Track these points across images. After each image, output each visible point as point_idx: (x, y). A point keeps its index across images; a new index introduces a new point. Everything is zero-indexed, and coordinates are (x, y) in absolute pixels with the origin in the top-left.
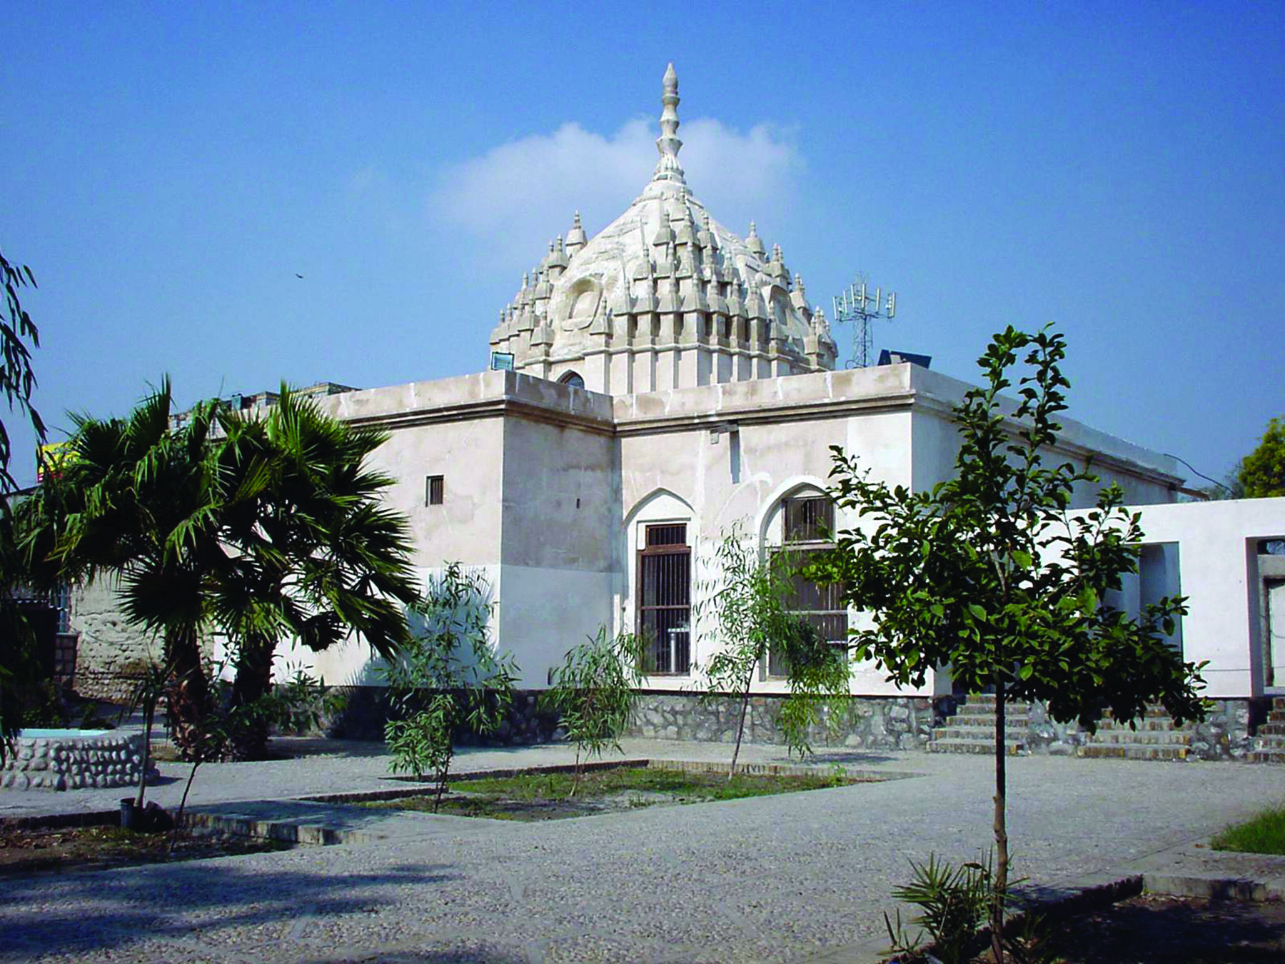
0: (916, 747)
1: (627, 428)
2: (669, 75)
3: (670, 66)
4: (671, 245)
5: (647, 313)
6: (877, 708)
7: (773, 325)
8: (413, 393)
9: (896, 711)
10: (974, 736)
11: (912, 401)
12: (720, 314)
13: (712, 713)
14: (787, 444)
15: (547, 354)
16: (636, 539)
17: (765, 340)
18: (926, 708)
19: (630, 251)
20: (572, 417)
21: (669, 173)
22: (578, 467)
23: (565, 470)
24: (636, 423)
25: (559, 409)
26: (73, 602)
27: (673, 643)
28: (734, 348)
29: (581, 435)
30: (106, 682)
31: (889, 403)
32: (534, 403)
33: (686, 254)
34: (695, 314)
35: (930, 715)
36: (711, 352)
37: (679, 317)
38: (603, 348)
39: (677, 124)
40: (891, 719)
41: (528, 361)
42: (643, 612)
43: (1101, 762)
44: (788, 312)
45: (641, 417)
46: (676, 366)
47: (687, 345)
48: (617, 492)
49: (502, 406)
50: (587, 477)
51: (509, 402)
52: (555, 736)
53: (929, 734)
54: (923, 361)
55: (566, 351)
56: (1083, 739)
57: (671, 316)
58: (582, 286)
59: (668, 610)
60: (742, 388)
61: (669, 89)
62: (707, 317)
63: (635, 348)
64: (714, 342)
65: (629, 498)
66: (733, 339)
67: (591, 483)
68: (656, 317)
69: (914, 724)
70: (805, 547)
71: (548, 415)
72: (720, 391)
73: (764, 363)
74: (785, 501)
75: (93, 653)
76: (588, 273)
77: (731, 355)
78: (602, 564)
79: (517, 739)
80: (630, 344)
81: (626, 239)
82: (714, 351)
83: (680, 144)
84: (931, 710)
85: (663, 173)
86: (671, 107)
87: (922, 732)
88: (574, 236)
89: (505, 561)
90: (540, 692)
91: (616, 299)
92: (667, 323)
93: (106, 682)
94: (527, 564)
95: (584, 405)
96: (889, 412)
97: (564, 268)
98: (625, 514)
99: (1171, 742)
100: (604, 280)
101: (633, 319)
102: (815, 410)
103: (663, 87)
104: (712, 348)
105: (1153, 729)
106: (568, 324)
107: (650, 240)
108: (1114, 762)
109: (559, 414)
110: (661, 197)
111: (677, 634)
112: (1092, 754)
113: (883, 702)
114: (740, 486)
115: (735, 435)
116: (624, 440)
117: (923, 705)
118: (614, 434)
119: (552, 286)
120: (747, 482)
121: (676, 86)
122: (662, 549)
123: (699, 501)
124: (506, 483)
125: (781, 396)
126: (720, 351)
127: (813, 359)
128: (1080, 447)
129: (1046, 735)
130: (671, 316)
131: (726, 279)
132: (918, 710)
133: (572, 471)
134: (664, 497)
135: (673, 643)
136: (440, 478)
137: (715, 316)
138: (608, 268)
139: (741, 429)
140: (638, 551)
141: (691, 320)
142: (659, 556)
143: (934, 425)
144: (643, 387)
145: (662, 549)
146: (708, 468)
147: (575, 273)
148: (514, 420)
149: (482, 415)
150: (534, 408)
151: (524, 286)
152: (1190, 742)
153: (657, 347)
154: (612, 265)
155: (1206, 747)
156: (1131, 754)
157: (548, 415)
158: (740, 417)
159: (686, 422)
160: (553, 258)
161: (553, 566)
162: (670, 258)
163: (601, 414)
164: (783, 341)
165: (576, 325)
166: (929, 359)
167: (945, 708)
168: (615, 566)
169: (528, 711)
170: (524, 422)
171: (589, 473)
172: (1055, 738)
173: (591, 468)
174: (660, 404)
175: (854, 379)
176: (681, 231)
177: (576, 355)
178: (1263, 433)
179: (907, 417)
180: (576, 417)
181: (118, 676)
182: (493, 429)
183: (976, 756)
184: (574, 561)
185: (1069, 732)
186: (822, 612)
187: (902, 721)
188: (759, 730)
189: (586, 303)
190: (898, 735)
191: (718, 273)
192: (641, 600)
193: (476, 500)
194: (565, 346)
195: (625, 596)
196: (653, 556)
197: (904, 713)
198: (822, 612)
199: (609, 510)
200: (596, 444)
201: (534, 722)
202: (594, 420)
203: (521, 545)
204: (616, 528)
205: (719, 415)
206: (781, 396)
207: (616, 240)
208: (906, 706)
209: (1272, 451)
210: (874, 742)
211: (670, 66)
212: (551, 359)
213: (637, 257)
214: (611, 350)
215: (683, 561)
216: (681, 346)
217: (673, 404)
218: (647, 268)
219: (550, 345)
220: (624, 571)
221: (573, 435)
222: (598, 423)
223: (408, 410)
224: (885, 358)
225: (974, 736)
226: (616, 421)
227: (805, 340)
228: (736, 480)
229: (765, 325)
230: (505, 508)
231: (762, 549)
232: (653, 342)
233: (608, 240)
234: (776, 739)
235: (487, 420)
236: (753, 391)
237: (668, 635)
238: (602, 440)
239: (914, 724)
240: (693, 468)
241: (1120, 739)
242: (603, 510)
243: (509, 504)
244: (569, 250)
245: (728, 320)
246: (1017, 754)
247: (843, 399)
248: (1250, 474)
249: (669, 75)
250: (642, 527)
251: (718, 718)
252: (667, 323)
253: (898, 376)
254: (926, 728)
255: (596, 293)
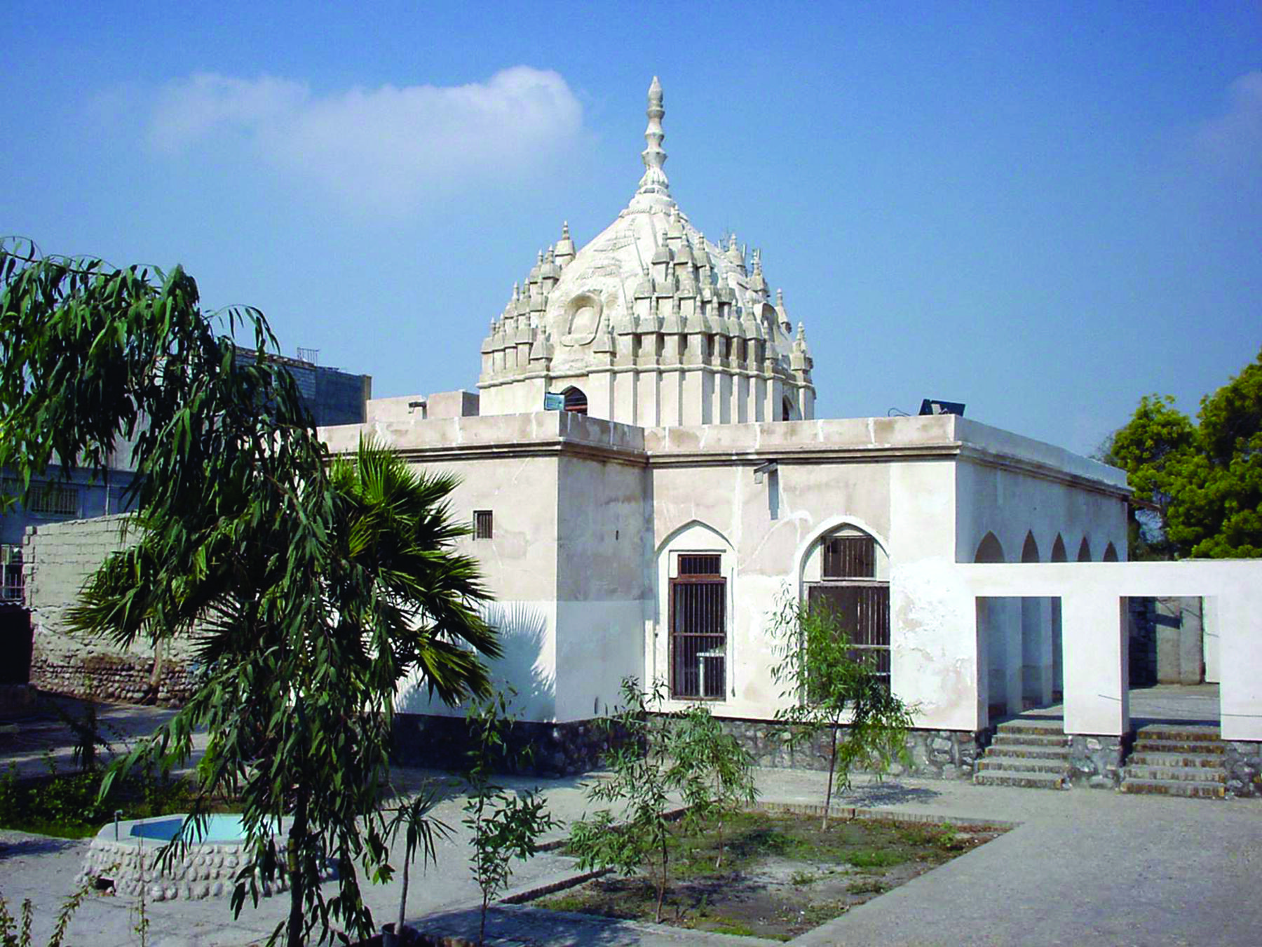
0: (959, 778)
1: (661, 460)
2: (654, 89)
3: (655, 79)
4: (671, 265)
5: (652, 333)
6: (920, 740)
7: (768, 345)
8: (457, 427)
9: (938, 743)
10: (1017, 769)
11: (958, 451)
12: (722, 335)
13: (750, 738)
14: (827, 485)
15: (548, 370)
16: (667, 568)
17: (761, 359)
18: (969, 741)
19: (626, 268)
20: (613, 452)
21: (656, 187)
22: (616, 500)
23: (608, 503)
24: (670, 456)
25: (605, 446)
26: (27, 594)
27: (702, 666)
28: (735, 369)
29: (619, 467)
30: (67, 675)
31: (934, 452)
32: (584, 442)
33: (685, 274)
34: (699, 337)
35: (972, 748)
36: (713, 373)
37: (684, 338)
38: (609, 367)
39: (662, 137)
40: (934, 750)
41: (527, 375)
42: (675, 638)
43: (1144, 799)
44: (775, 327)
45: (676, 451)
46: (680, 385)
47: (692, 366)
48: (648, 521)
49: (558, 447)
50: (623, 509)
51: (565, 444)
52: (600, 763)
53: (972, 766)
54: (957, 409)
55: (567, 366)
56: (1122, 774)
57: (676, 337)
58: (581, 302)
59: (701, 637)
60: (782, 426)
61: (655, 102)
62: (709, 338)
63: (639, 368)
64: (716, 363)
65: (661, 528)
66: (733, 358)
67: (627, 512)
68: (661, 337)
69: (957, 756)
70: (844, 584)
71: (595, 454)
72: (758, 430)
73: (760, 381)
74: (823, 539)
75: (51, 647)
76: (586, 289)
77: (732, 375)
78: (636, 592)
79: (571, 769)
80: (635, 364)
81: (621, 254)
82: (718, 372)
83: (665, 157)
84: (973, 743)
85: (649, 186)
86: (657, 120)
87: (964, 763)
88: (563, 247)
89: (559, 598)
90: (589, 721)
91: (619, 316)
92: (672, 343)
93: (67, 675)
94: (576, 599)
95: (622, 439)
96: (934, 460)
97: (556, 280)
98: (657, 544)
99: (1207, 780)
100: (603, 297)
101: (638, 339)
102: (859, 455)
103: (649, 100)
104: (715, 368)
105: (1186, 765)
106: (567, 339)
107: (648, 258)
108: (1159, 798)
109: (605, 450)
110: (649, 211)
111: (706, 658)
112: (1135, 790)
113: (925, 734)
114: (778, 524)
115: (773, 475)
116: (655, 471)
117: (965, 739)
118: (646, 464)
119: (547, 298)
120: (786, 520)
121: (661, 99)
122: (694, 579)
123: (735, 531)
124: (561, 520)
125: (821, 438)
126: (722, 372)
127: (800, 375)
128: (1066, 474)
129: (1086, 770)
130: (676, 337)
131: (724, 299)
132: (961, 743)
133: (612, 504)
134: (698, 529)
135: (702, 666)
136: (490, 513)
137: (717, 338)
138: (607, 285)
139: (780, 468)
140: (670, 579)
141: (696, 342)
142: (691, 585)
143: (969, 469)
144: (670, 420)
145: (694, 579)
146: (746, 503)
147: (570, 286)
148: (565, 459)
149: (535, 454)
150: (584, 447)
151: (515, 296)
152: (1224, 780)
153: (662, 367)
154: (611, 281)
155: (1239, 784)
156: (1173, 791)
157: (595, 454)
158: (780, 456)
159: (724, 458)
160: (546, 269)
161: (597, 599)
162: (670, 278)
163: (634, 445)
164: (775, 360)
165: (577, 341)
166: (963, 406)
167: (983, 740)
168: (648, 593)
169: (579, 741)
170: (575, 460)
171: (626, 504)
172: (1095, 772)
173: (628, 499)
174: (695, 438)
175: (897, 427)
176: (680, 251)
177: (578, 372)
178: (1135, 408)
179: (950, 466)
180: (619, 453)
181: (77, 670)
182: (548, 467)
183: (1023, 790)
184: (614, 591)
185: (1109, 767)
186: (862, 646)
187: (945, 752)
188: (798, 756)
189: (585, 317)
190: (939, 765)
191: (716, 293)
192: (673, 628)
193: (528, 537)
194: (566, 362)
195: (657, 622)
196: (686, 585)
197: (947, 745)
198: (862, 646)
199: (642, 539)
200: (631, 476)
201: (584, 751)
202: (629, 454)
203: (574, 582)
204: (648, 556)
205: (758, 453)
206: (821, 438)
207: (611, 254)
208: (949, 739)
209: (1144, 426)
210: (917, 771)
211: (655, 79)
212: (552, 374)
213: (636, 275)
214: (616, 368)
215: (718, 591)
216: (685, 367)
217: (710, 439)
218: (648, 286)
219: (549, 360)
220: (656, 597)
221: (613, 469)
222: (634, 456)
223: (454, 445)
224: (926, 409)
225: (1017, 769)
226: (649, 453)
227: (791, 356)
228: (774, 516)
229: (761, 344)
230: (560, 546)
231: (802, 583)
232: (658, 362)
233: (602, 255)
234: (816, 765)
235: (541, 459)
236: (793, 432)
237: (697, 659)
238: (636, 470)
239: (957, 756)
240: (729, 502)
241: (1158, 776)
242: (637, 540)
243: (564, 542)
244: (559, 261)
245: (728, 341)
246: (1062, 789)
247: (887, 446)
248: (1122, 447)
249: (654, 89)
250: (674, 556)
251: (756, 744)
252: (672, 343)
253: (943, 426)
254: (969, 760)
255: (597, 309)
